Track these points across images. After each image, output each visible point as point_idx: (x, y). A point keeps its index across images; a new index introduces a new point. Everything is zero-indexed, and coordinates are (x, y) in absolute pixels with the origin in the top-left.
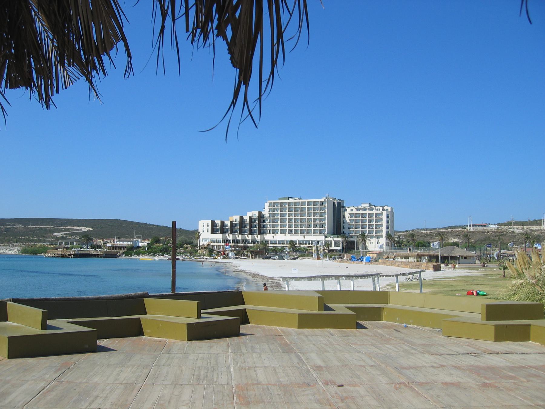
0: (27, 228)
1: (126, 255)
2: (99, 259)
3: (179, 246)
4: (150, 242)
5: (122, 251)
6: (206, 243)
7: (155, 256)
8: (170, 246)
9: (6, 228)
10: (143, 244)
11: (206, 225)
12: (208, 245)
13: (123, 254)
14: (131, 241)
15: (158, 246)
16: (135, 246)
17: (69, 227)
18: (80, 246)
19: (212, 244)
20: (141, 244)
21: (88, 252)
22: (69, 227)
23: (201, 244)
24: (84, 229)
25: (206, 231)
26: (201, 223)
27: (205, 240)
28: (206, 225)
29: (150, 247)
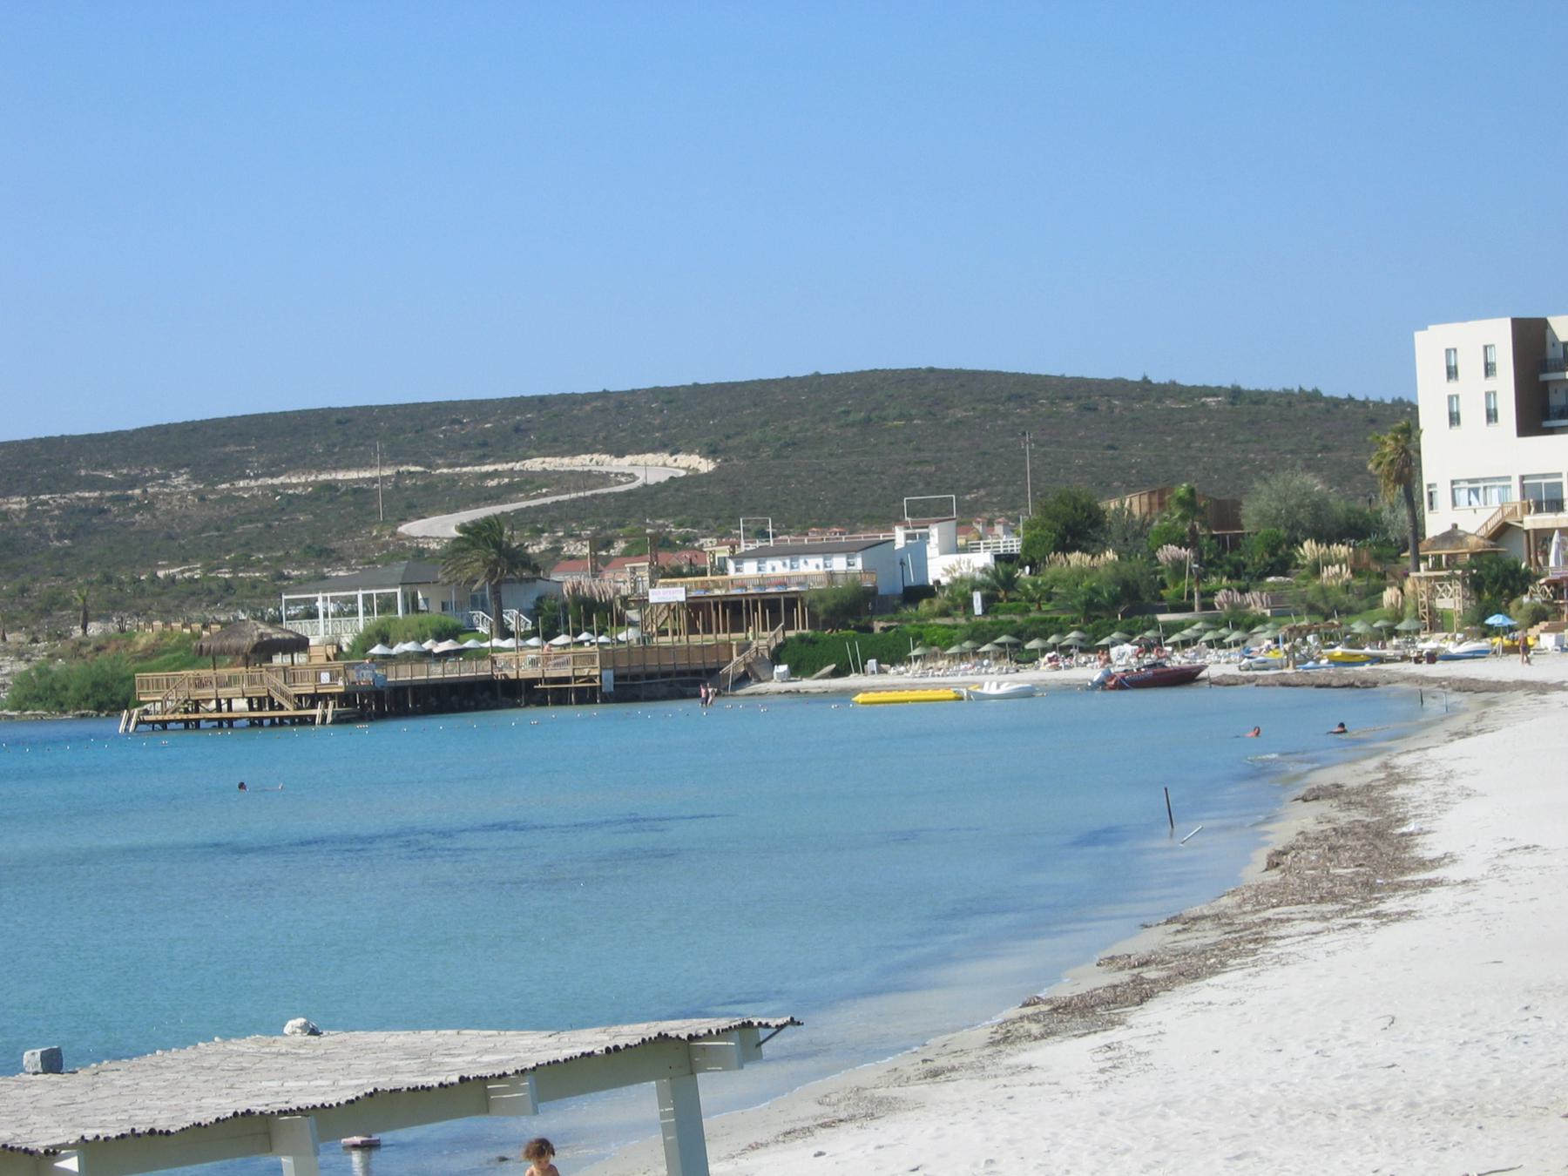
0: (228, 498)
1: (797, 671)
2: (552, 713)
3: (1257, 556)
4: (1014, 544)
5: (763, 639)
6: (1475, 521)
7: (1032, 658)
8: (1178, 567)
9: (70, 510)
10: (949, 560)
11: (1470, 366)
12: (1503, 531)
13: (776, 658)
14: (849, 551)
15: (1083, 573)
16: (889, 585)
17: (535, 464)
18: (452, 619)
19: (1532, 521)
20: (940, 566)
21: (482, 669)
22: (535, 464)
23: (1435, 524)
24: (652, 468)
25: (1472, 412)
26: (1430, 344)
27: (1476, 487)
28: (1470, 366)
29: (1009, 583)
